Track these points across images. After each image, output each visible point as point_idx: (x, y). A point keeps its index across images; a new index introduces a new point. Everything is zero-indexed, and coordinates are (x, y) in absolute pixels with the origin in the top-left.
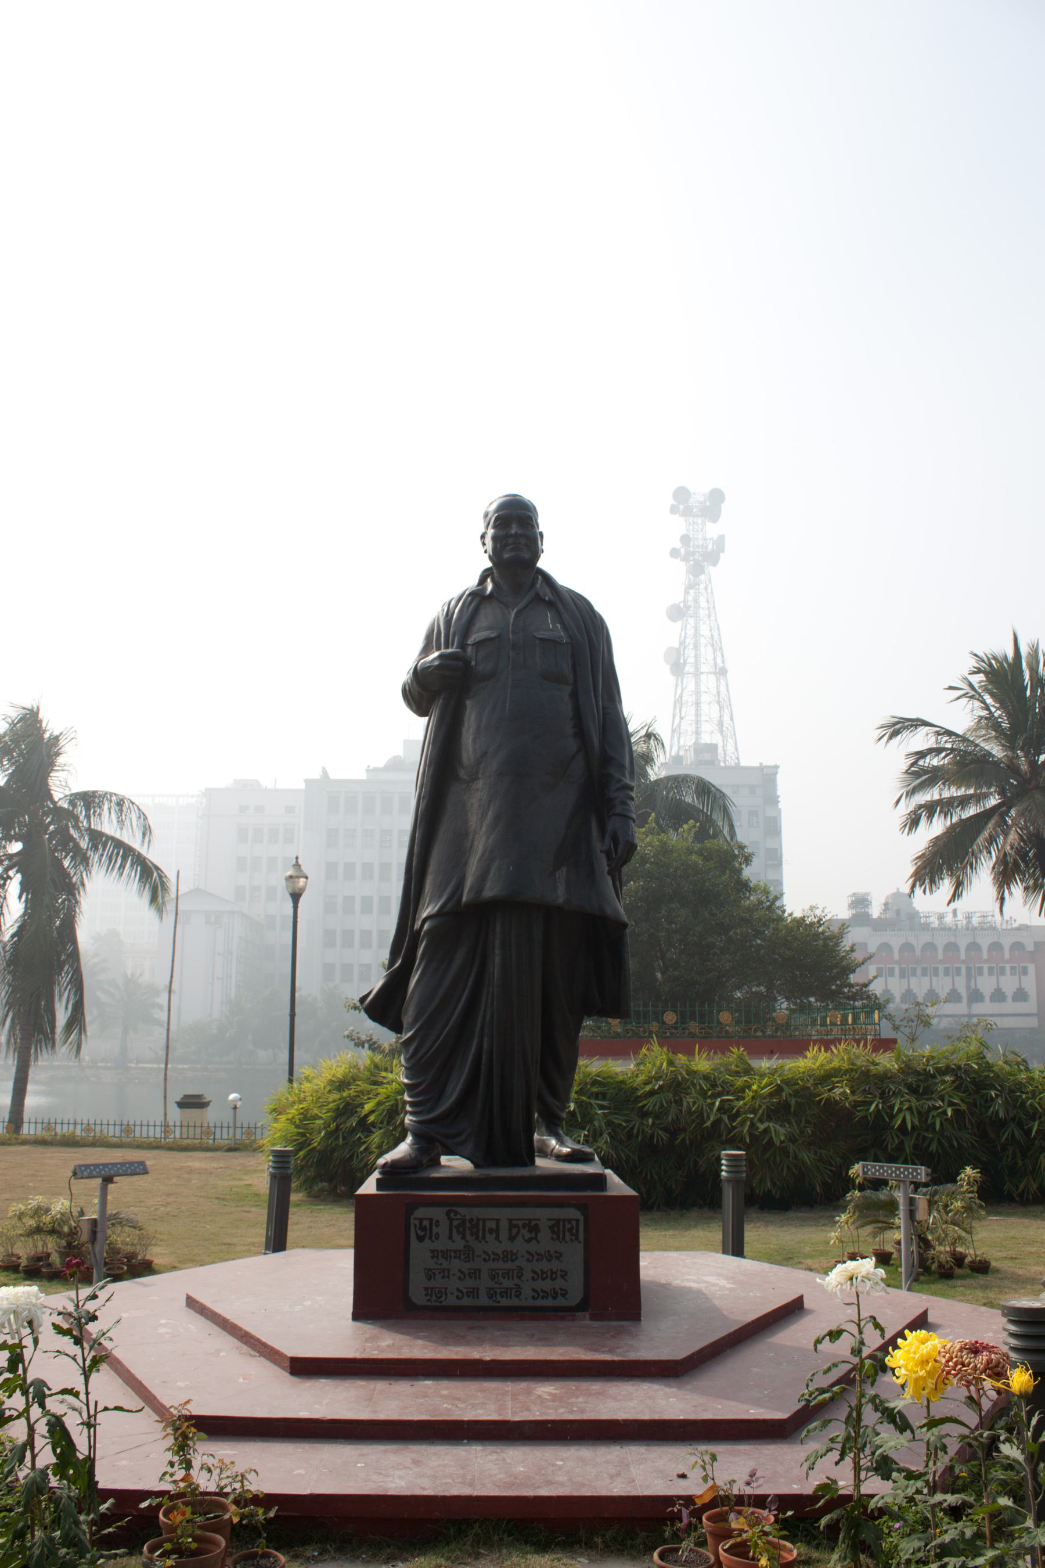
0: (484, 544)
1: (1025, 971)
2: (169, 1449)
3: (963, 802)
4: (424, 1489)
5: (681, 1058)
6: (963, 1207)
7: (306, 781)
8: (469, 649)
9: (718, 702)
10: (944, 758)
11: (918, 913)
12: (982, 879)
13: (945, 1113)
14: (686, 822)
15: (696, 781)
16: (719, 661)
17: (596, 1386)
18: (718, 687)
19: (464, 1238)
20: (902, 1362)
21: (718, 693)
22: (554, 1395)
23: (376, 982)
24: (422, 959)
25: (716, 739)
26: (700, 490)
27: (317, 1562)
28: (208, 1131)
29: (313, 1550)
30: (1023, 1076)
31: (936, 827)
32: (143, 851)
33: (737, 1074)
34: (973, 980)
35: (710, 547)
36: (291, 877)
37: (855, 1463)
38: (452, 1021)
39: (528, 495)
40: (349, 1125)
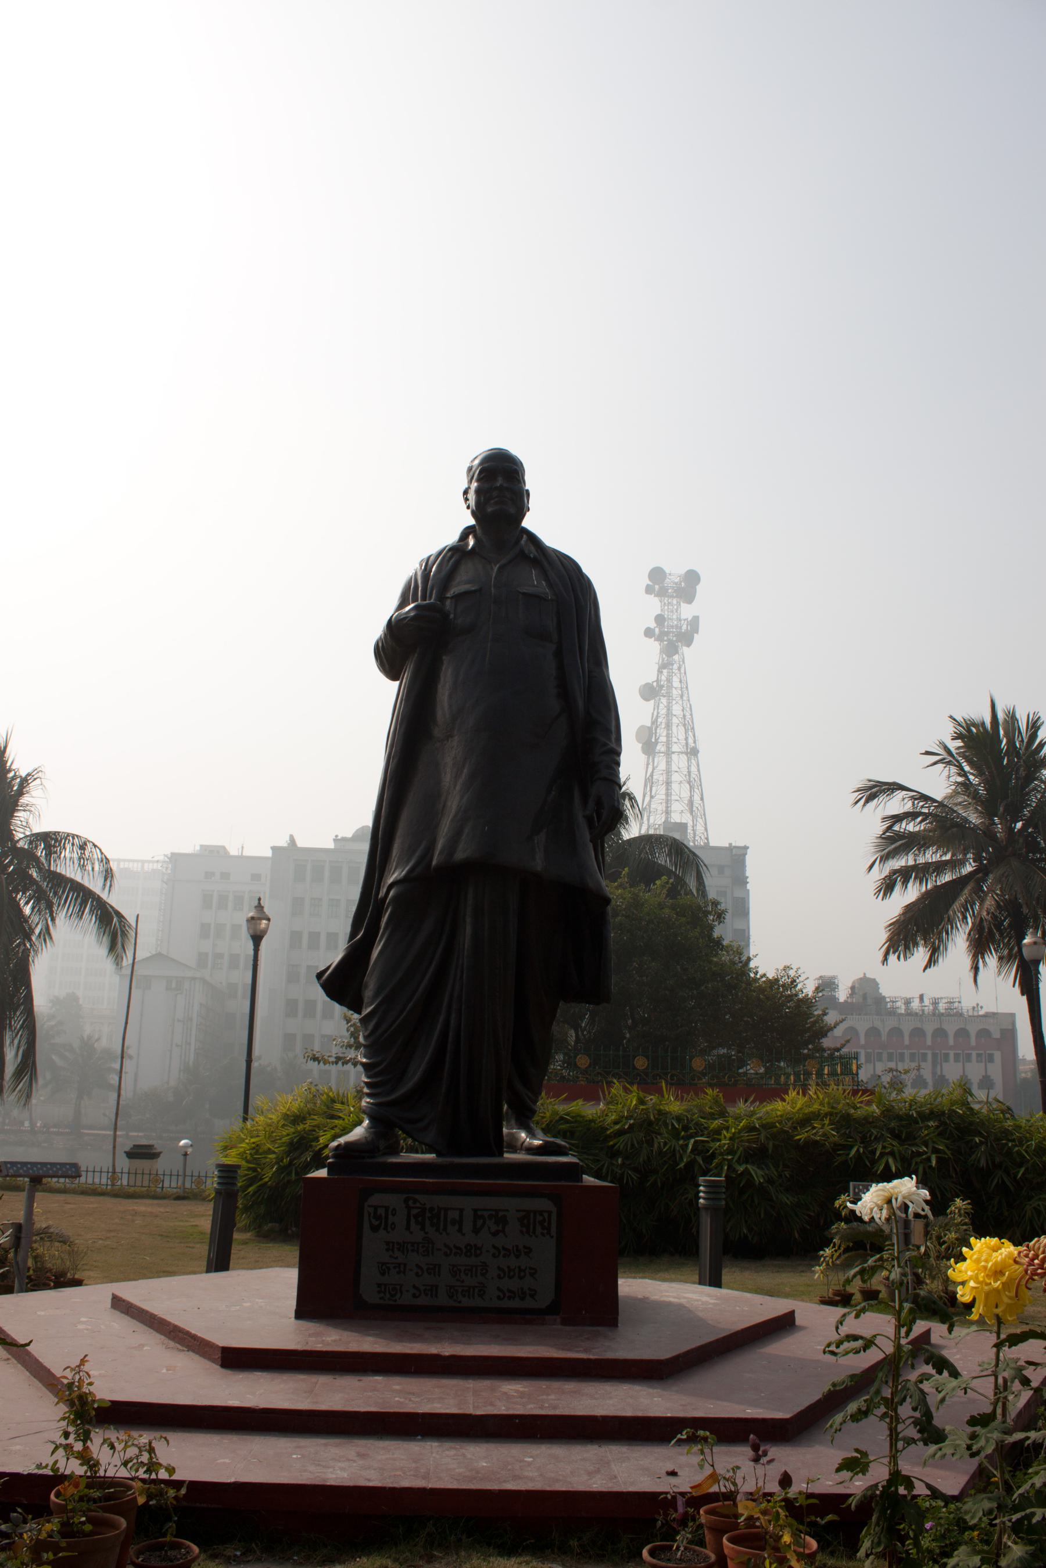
0: (466, 500)
1: (991, 1059)
2: (63, 1419)
3: (939, 867)
4: (369, 1480)
5: (652, 1099)
6: (957, 1239)
7: (274, 848)
8: (448, 602)
9: (689, 782)
10: (921, 822)
11: (884, 998)
12: (958, 945)
13: (929, 1159)
14: (659, 878)
15: (669, 843)
16: (691, 741)
17: (570, 1386)
18: (689, 767)
19: (423, 1229)
20: (970, 1273)
21: (689, 772)
22: (522, 1393)
23: (335, 957)
24: (386, 928)
25: (686, 818)
26: (676, 570)
27: (239, 1563)
28: (156, 1179)
29: (236, 1549)
30: (1009, 1124)
31: (910, 894)
32: (104, 896)
33: (712, 1116)
34: (939, 1067)
35: (684, 627)
36: (253, 918)
37: (891, 1430)
38: (421, 990)
39: (515, 451)
40: (303, 1159)
